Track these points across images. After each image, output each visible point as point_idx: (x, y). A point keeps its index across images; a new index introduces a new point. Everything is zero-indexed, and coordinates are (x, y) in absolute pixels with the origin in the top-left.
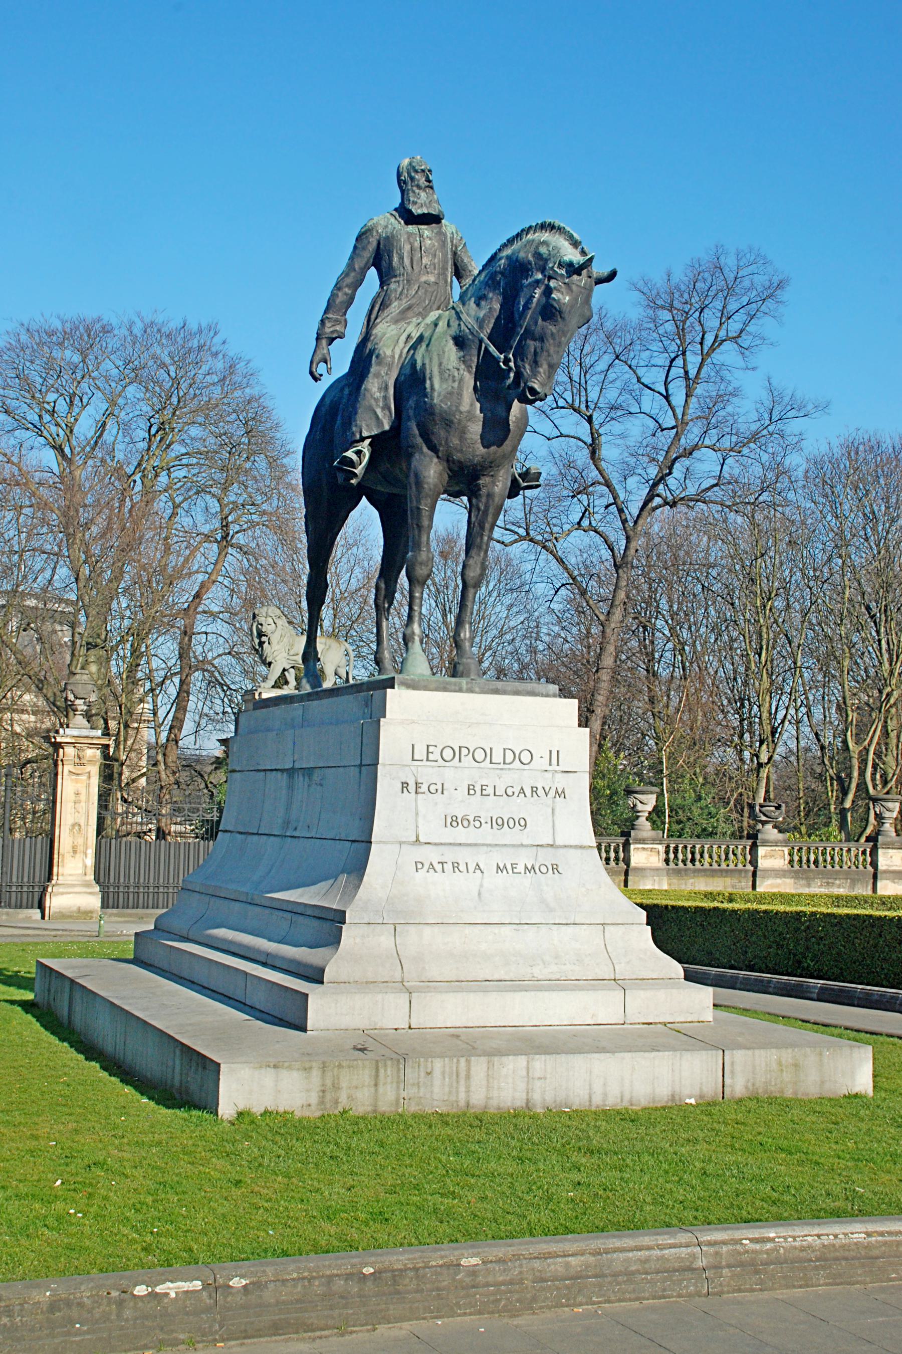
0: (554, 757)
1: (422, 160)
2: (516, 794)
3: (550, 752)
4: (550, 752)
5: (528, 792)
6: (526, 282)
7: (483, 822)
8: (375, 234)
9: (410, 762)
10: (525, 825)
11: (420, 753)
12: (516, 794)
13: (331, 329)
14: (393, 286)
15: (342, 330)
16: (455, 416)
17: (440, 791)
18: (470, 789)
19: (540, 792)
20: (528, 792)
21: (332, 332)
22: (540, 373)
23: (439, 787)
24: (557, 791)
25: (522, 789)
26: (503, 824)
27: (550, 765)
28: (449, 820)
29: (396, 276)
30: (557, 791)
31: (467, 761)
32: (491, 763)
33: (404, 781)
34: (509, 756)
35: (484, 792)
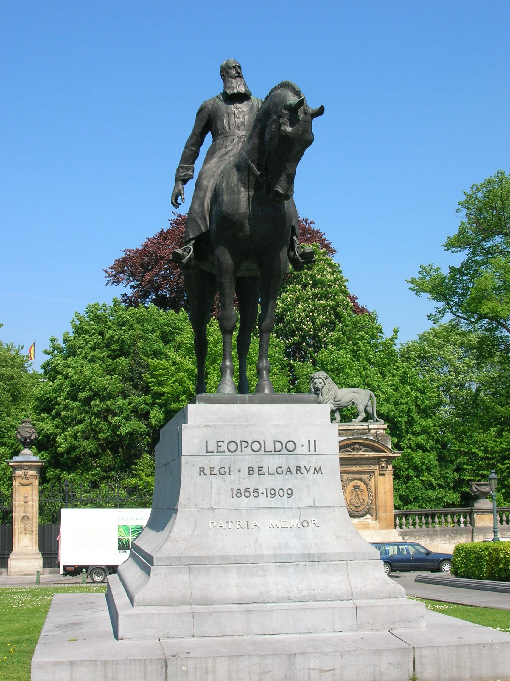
0: (312, 445)
1: (232, 59)
2: (284, 472)
3: (309, 441)
4: (309, 441)
5: (294, 470)
6: (269, 122)
7: (260, 492)
8: (207, 110)
9: (205, 453)
10: (292, 494)
11: (212, 447)
12: (284, 472)
13: (184, 174)
14: (218, 141)
15: (191, 173)
16: (235, 217)
17: (227, 473)
18: (251, 470)
19: (303, 470)
20: (294, 470)
21: (185, 176)
22: (281, 181)
23: (227, 470)
24: (315, 469)
25: (289, 468)
26: (275, 494)
27: (310, 451)
28: (235, 492)
29: (219, 135)
30: (315, 469)
31: (248, 451)
32: (265, 452)
33: (250, 466)
34: (278, 446)
35: (261, 472)
